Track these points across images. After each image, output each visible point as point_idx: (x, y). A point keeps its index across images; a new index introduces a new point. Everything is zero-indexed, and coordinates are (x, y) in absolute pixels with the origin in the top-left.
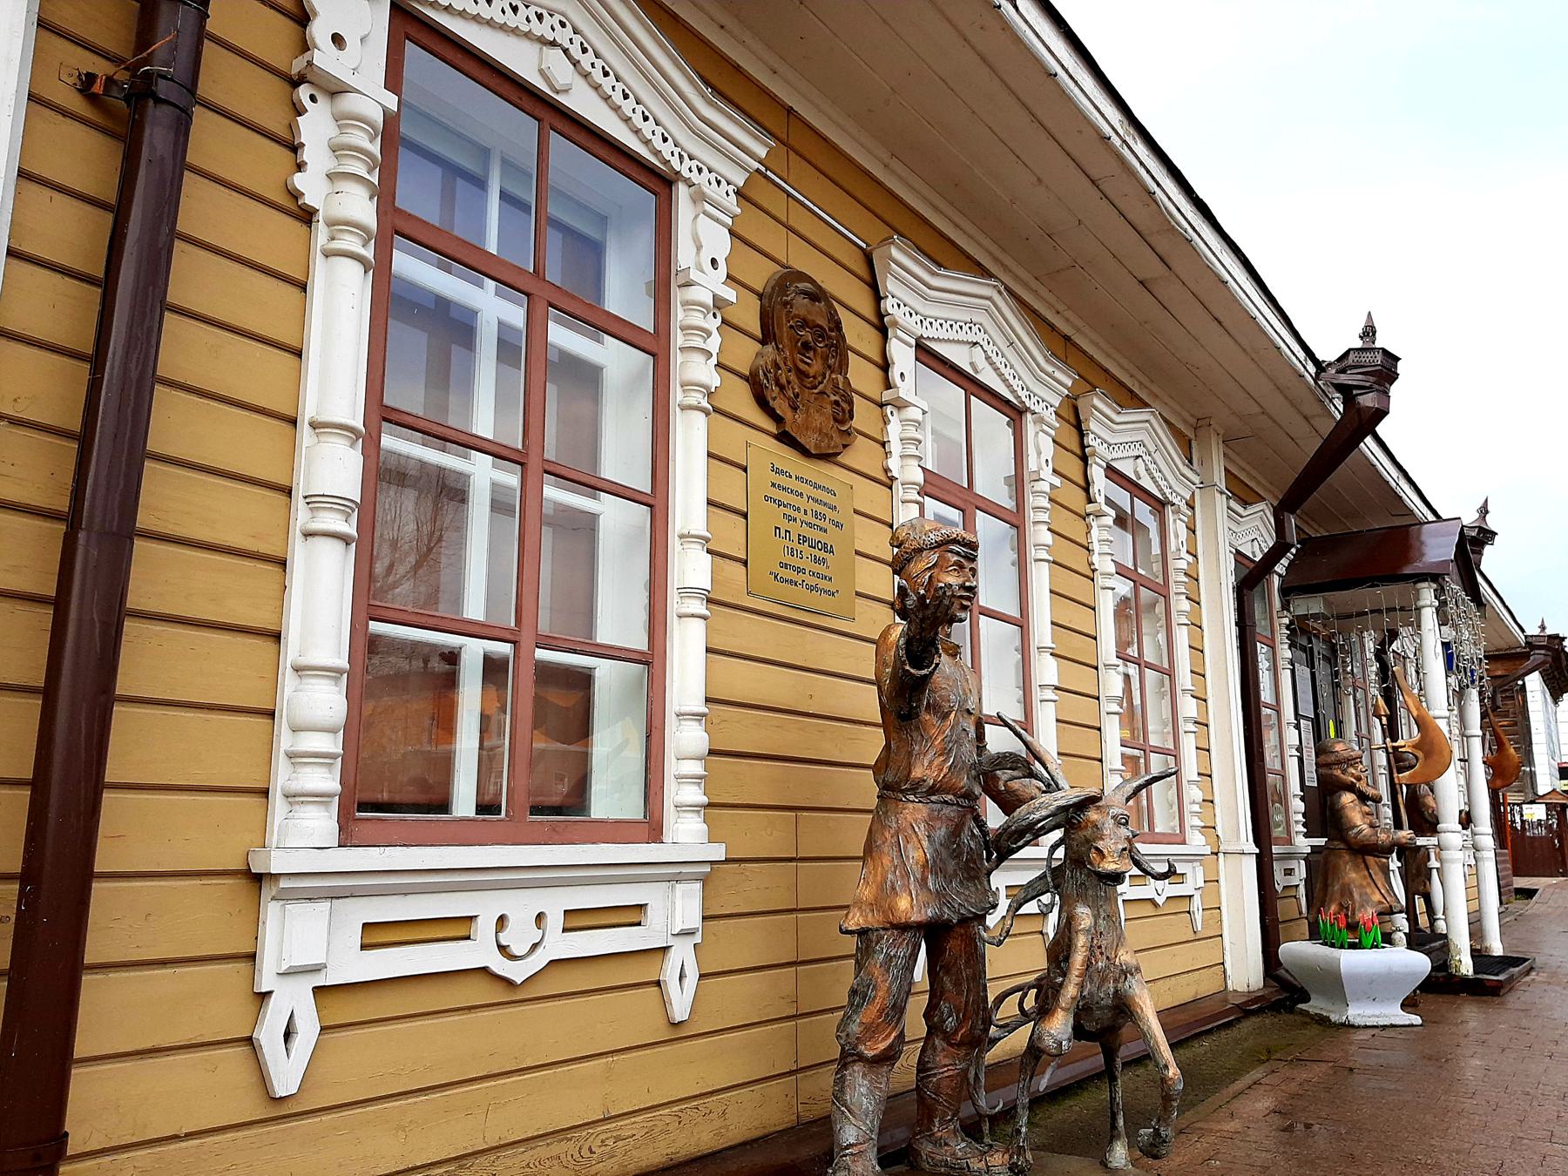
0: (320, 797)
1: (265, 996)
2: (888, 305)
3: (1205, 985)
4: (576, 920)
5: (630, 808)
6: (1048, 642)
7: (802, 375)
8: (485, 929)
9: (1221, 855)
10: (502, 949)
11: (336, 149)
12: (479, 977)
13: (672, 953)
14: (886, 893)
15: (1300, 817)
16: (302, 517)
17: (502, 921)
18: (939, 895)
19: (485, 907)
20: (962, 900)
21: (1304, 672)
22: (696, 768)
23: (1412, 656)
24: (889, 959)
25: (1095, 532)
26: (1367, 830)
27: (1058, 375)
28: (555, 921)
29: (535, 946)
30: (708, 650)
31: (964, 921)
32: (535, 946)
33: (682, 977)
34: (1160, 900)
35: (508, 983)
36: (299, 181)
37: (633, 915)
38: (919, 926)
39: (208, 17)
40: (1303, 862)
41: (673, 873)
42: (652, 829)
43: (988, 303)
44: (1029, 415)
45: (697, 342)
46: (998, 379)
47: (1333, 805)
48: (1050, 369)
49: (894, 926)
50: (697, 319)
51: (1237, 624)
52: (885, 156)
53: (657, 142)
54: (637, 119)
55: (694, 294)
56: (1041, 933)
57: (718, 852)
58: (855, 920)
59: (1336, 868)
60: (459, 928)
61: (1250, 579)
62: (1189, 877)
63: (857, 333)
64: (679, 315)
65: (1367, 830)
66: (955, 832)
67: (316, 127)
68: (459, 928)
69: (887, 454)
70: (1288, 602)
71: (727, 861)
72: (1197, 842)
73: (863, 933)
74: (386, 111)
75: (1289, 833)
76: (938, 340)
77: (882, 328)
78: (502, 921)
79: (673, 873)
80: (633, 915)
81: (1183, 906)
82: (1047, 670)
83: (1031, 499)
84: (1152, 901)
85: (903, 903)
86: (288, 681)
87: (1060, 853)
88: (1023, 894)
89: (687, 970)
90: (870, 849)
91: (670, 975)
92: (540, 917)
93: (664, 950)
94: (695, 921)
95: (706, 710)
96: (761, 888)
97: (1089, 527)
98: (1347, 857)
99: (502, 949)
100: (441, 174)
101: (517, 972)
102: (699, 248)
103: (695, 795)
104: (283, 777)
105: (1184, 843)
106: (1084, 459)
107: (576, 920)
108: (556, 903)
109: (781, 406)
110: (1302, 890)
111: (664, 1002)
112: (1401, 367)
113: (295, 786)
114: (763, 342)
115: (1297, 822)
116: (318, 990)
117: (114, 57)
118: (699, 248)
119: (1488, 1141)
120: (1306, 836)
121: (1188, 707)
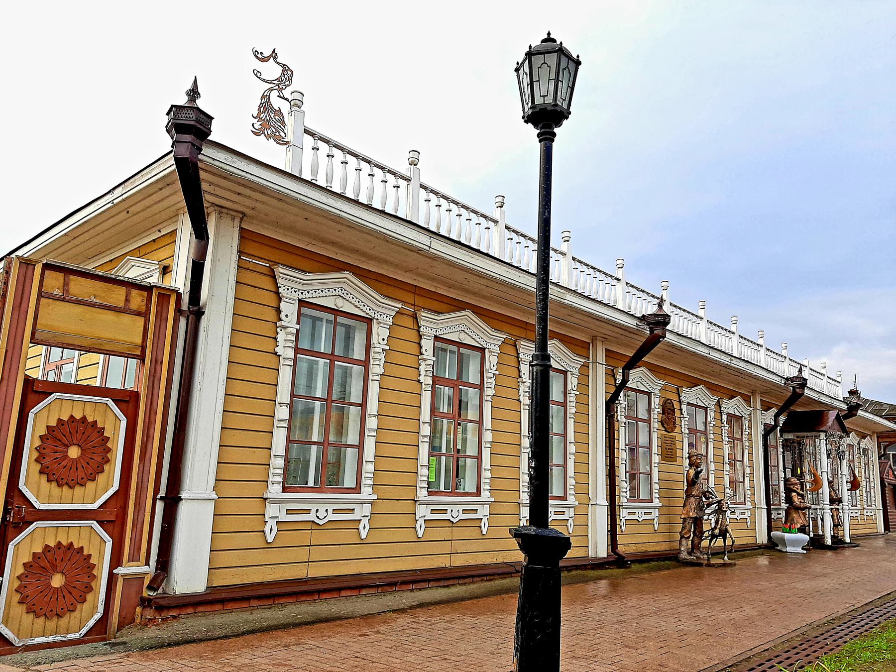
0: (278, 482)
1: (520, 520)
2: (682, 398)
3: (751, 541)
5: (647, 497)
6: (489, 427)
7: (668, 418)
8: (313, 512)
9: (590, 505)
10: (318, 517)
11: (426, 371)
12: (448, 521)
14: (688, 512)
15: (784, 498)
16: (276, 423)
17: (452, 511)
18: (696, 513)
20: (700, 514)
21: (788, 455)
22: (488, 481)
23: (870, 448)
24: (689, 522)
25: (723, 431)
26: (798, 503)
28: (330, 511)
29: (325, 517)
31: (700, 517)
32: (325, 517)
33: (271, 530)
34: (738, 519)
35: (453, 522)
36: (277, 349)
37: (563, 513)
38: (692, 518)
40: (784, 511)
41: (483, 504)
42: (478, 493)
43: (345, 279)
44: (375, 320)
45: (377, 362)
47: (790, 496)
49: (689, 517)
50: (377, 356)
51: (763, 446)
52: (447, 288)
53: (368, 311)
54: (362, 307)
55: (376, 350)
56: (566, 525)
57: (661, 505)
58: (683, 516)
59: (790, 513)
60: (308, 511)
61: (768, 431)
62: (746, 514)
63: (676, 405)
64: (568, 399)
65: (798, 503)
66: (699, 503)
67: (281, 337)
68: (308, 511)
69: (682, 428)
70: (783, 435)
71: (377, 499)
72: (749, 505)
73: (684, 518)
74: (297, 329)
75: (780, 503)
77: (680, 402)
79: (483, 504)
81: (781, 520)
82: (572, 449)
83: (486, 379)
84: (736, 518)
85: (691, 514)
87: (717, 508)
88: (710, 514)
90: (685, 505)
91: (361, 527)
92: (327, 511)
93: (360, 520)
94: (658, 515)
95: (490, 468)
96: (664, 512)
97: (722, 430)
98: (793, 511)
99: (318, 517)
101: (321, 522)
102: (379, 335)
103: (370, 482)
104: (271, 478)
105: (745, 505)
106: (721, 413)
107: (335, 511)
108: (331, 507)
109: (666, 426)
110: (784, 519)
111: (654, 527)
114: (662, 414)
115: (783, 500)
116: (277, 522)
117: (91, 304)
118: (572, 384)
120: (785, 504)
121: (748, 470)
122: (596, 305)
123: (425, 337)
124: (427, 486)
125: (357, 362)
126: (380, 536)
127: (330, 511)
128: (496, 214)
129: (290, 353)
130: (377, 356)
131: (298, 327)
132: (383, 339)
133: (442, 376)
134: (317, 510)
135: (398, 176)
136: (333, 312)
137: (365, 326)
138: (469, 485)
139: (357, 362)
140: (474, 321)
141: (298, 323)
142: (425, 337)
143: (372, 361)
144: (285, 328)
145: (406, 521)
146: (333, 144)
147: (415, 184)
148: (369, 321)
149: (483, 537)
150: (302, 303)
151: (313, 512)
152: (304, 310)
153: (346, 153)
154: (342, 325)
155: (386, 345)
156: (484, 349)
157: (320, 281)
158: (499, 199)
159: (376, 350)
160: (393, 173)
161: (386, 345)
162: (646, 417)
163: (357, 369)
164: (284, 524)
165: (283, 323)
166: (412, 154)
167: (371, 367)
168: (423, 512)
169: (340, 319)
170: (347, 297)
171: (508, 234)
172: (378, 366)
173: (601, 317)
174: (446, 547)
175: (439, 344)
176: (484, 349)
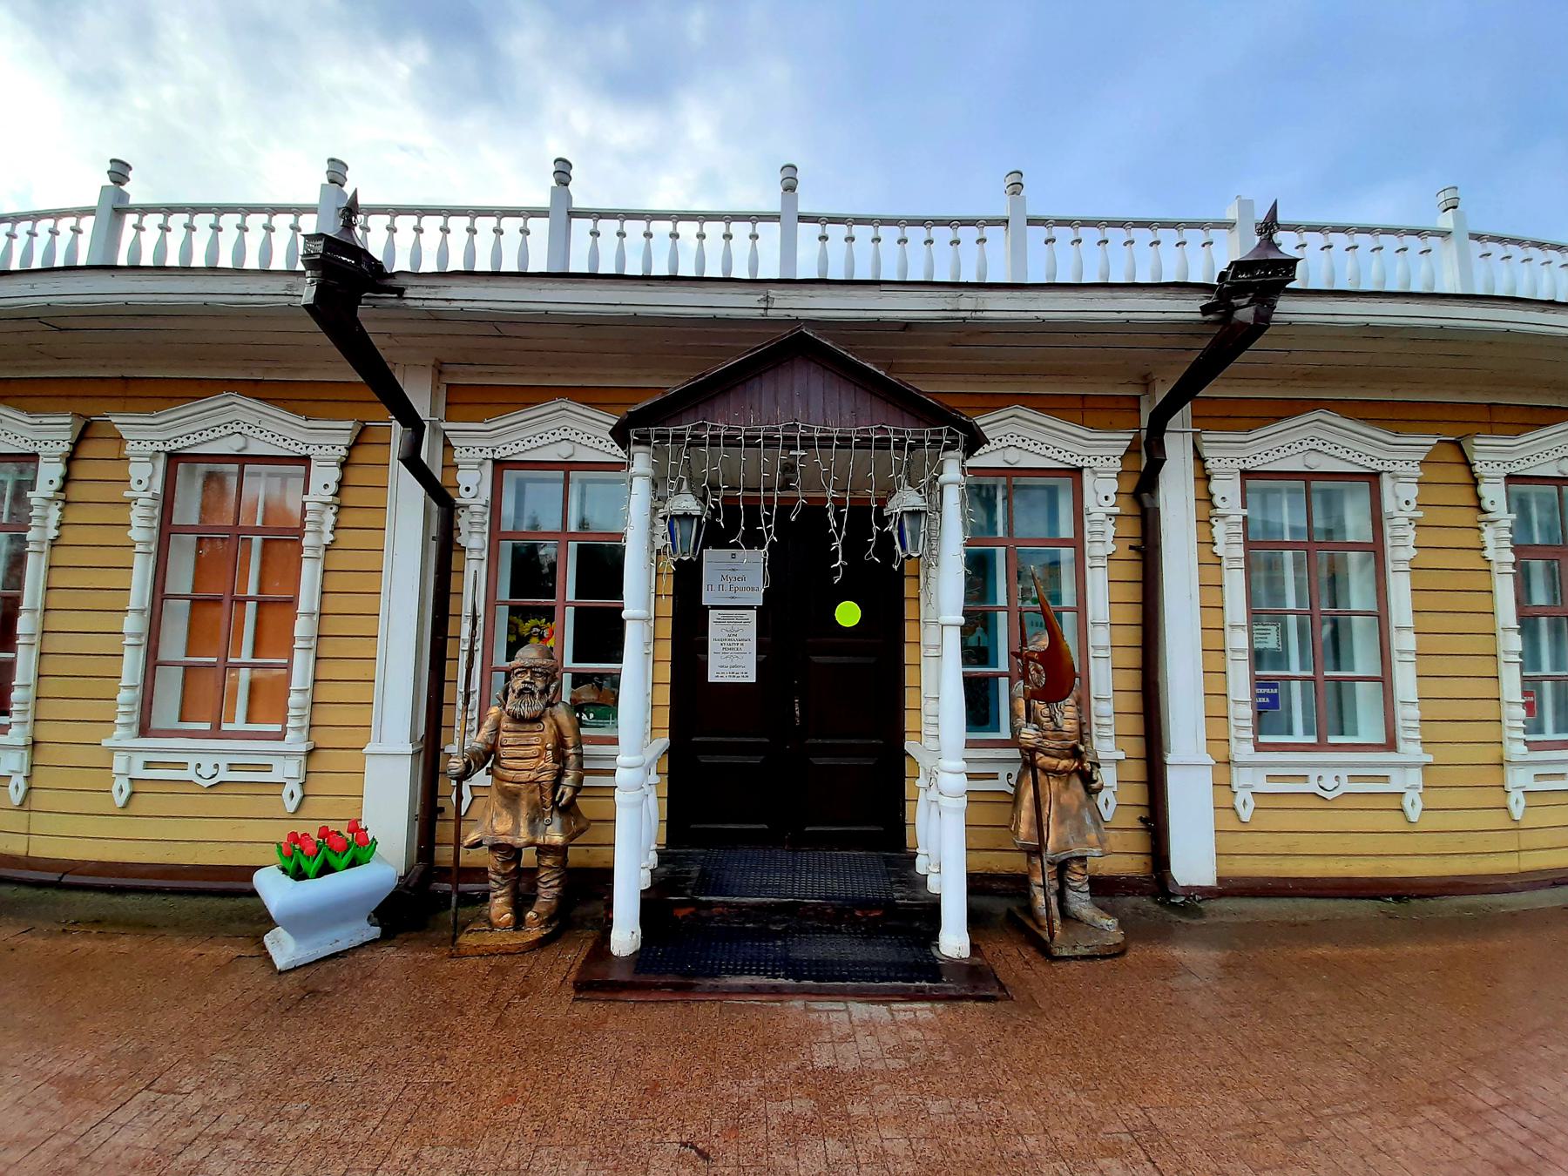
4: (232, 767)
8: (191, 766)
13: (1406, 796)
17: (199, 766)
19: (192, 760)
27: (45, 421)
28: (223, 767)
30: (1418, 676)
39: (1416, 498)
42: (1391, 745)
43: (234, 405)
46: (1343, 463)
48: (37, 421)
55: (1093, 517)
60: (183, 765)
68: (183, 765)
76: (190, 446)
78: (199, 766)
80: (267, 768)
86: (1231, 705)
89: (1416, 801)
91: (1407, 804)
92: (216, 766)
100: (280, 482)
101: (1329, 796)
102: (1397, 497)
107: (232, 767)
112: (131, 175)
113: (1404, 736)
116: (471, 786)
119: (930, 1040)
122: (833, 296)
123: (1486, 480)
124: (1252, 736)
125: (1065, 543)
126: (1537, 818)
127: (1344, 779)
128: (1446, 221)
129: (1239, 551)
130: (1400, 532)
131: (1245, 512)
132: (1106, 498)
133: (1261, 540)
134: (1320, 777)
135: (850, 221)
136: (1553, 482)
137: (1363, 489)
138: (1368, 728)
139: (1065, 543)
140: (223, 406)
141: (1244, 506)
142: (1486, 480)
143: (1087, 537)
144: (1224, 517)
145: (1493, 797)
146: (1077, 224)
147: (1018, 222)
148: (1373, 478)
149: (1516, 824)
150: (1246, 474)
151: (191, 766)
152: (1250, 483)
153: (956, 227)
154: (1256, 491)
155: (1113, 506)
156: (1079, 470)
157: (1060, 434)
158: (1015, 178)
159: (1397, 522)
160: (948, 223)
161: (1113, 506)
162: (1367, 537)
163: (1066, 554)
164: (144, 783)
165: (1219, 511)
166: (788, 172)
167: (1087, 545)
168: (1519, 779)
169: (1315, 485)
170: (1325, 449)
171: (1477, 248)
172: (1100, 544)
173: (107, 305)
174: (1510, 842)
175: (1515, 488)
176: (1079, 470)
